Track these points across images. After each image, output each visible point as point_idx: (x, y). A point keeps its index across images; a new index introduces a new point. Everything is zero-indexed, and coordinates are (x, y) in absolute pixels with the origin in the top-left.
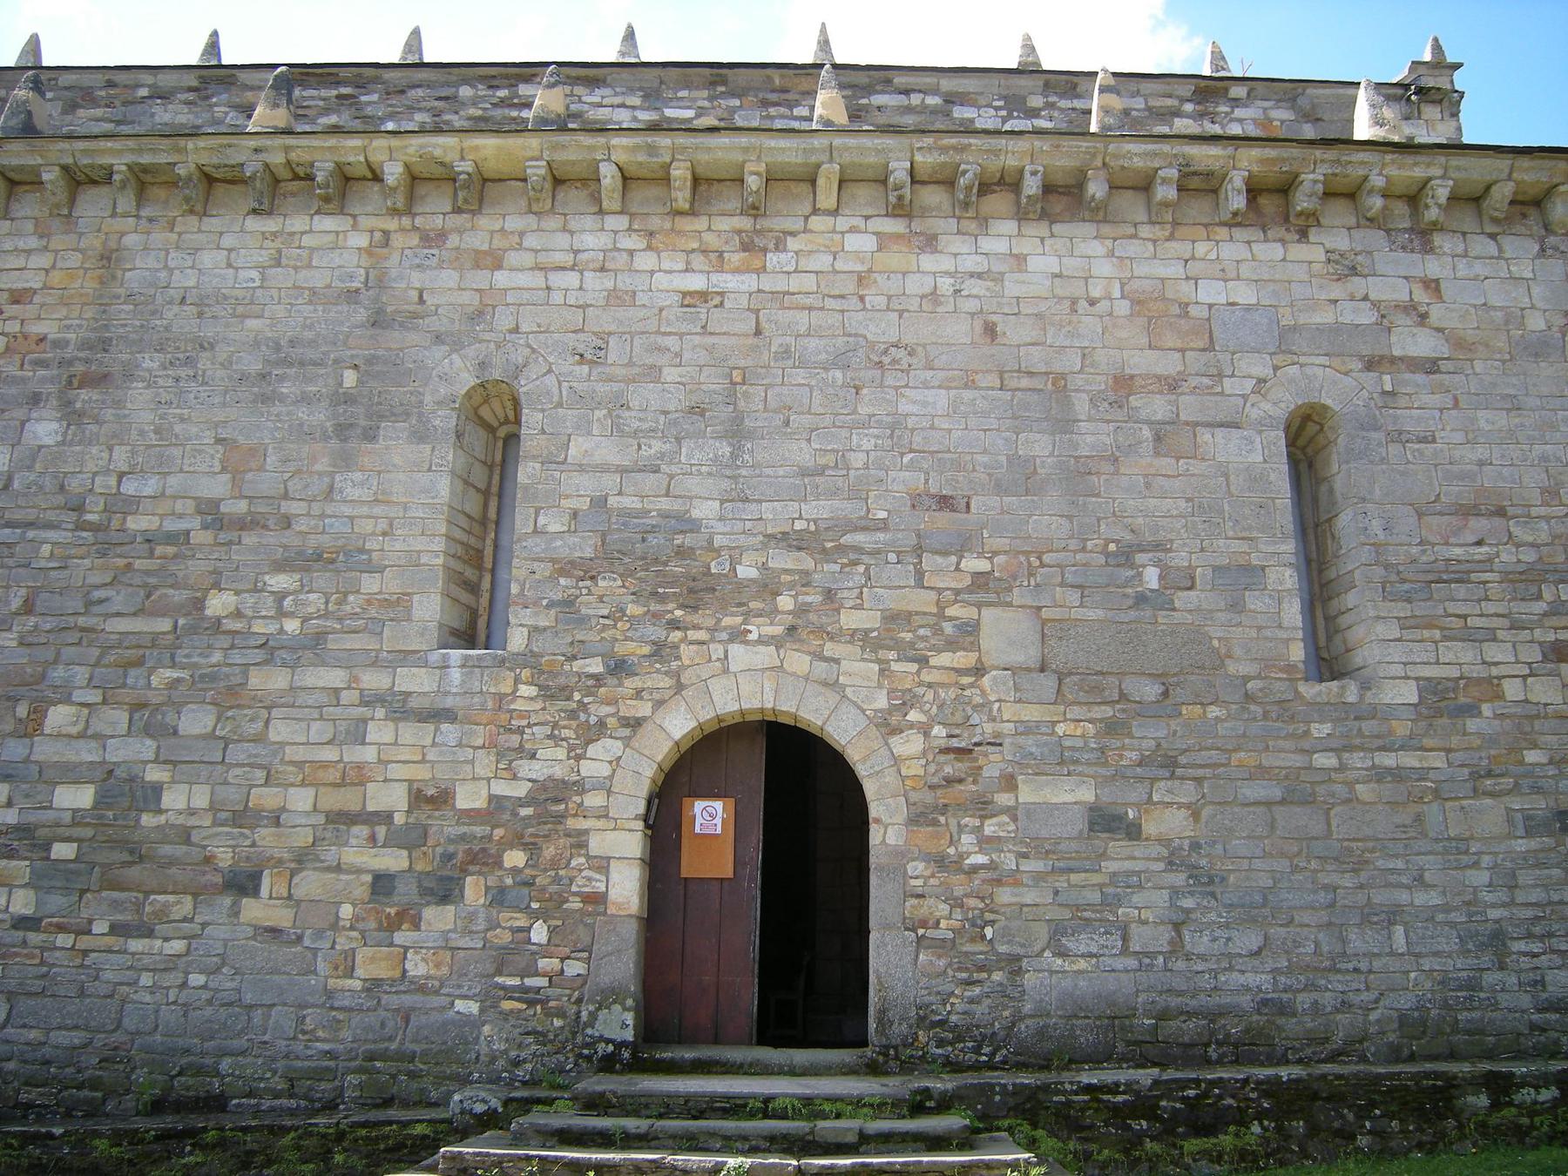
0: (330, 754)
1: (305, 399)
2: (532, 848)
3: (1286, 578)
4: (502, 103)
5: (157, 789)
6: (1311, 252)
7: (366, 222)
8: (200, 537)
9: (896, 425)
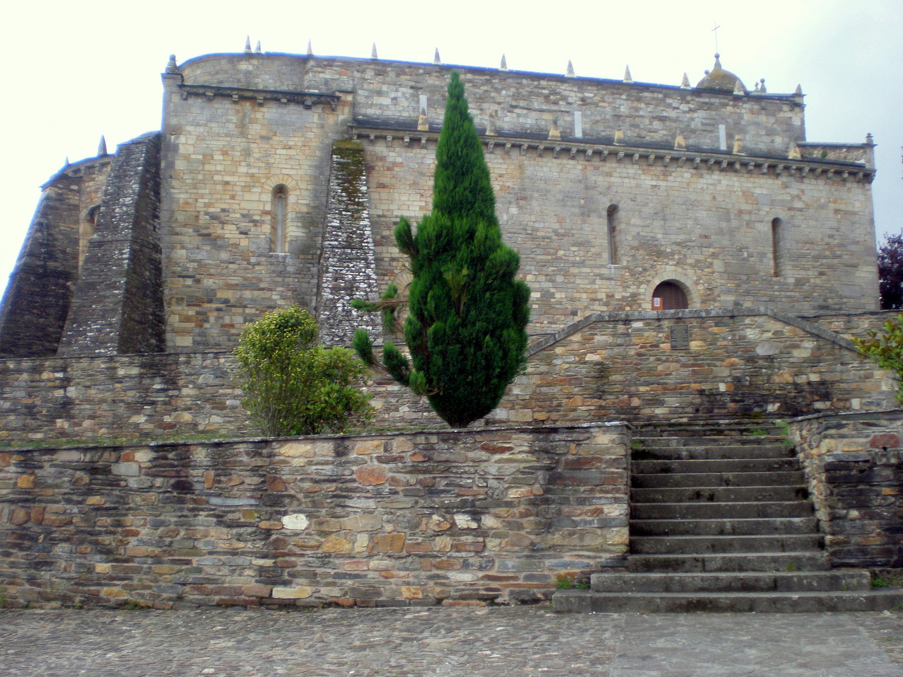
0: (589, 286)
1: (573, 206)
2: (630, 306)
3: (771, 256)
4: (536, 87)
5: (553, 294)
6: (779, 182)
7: (581, 162)
8: (555, 238)
9: (696, 219)
